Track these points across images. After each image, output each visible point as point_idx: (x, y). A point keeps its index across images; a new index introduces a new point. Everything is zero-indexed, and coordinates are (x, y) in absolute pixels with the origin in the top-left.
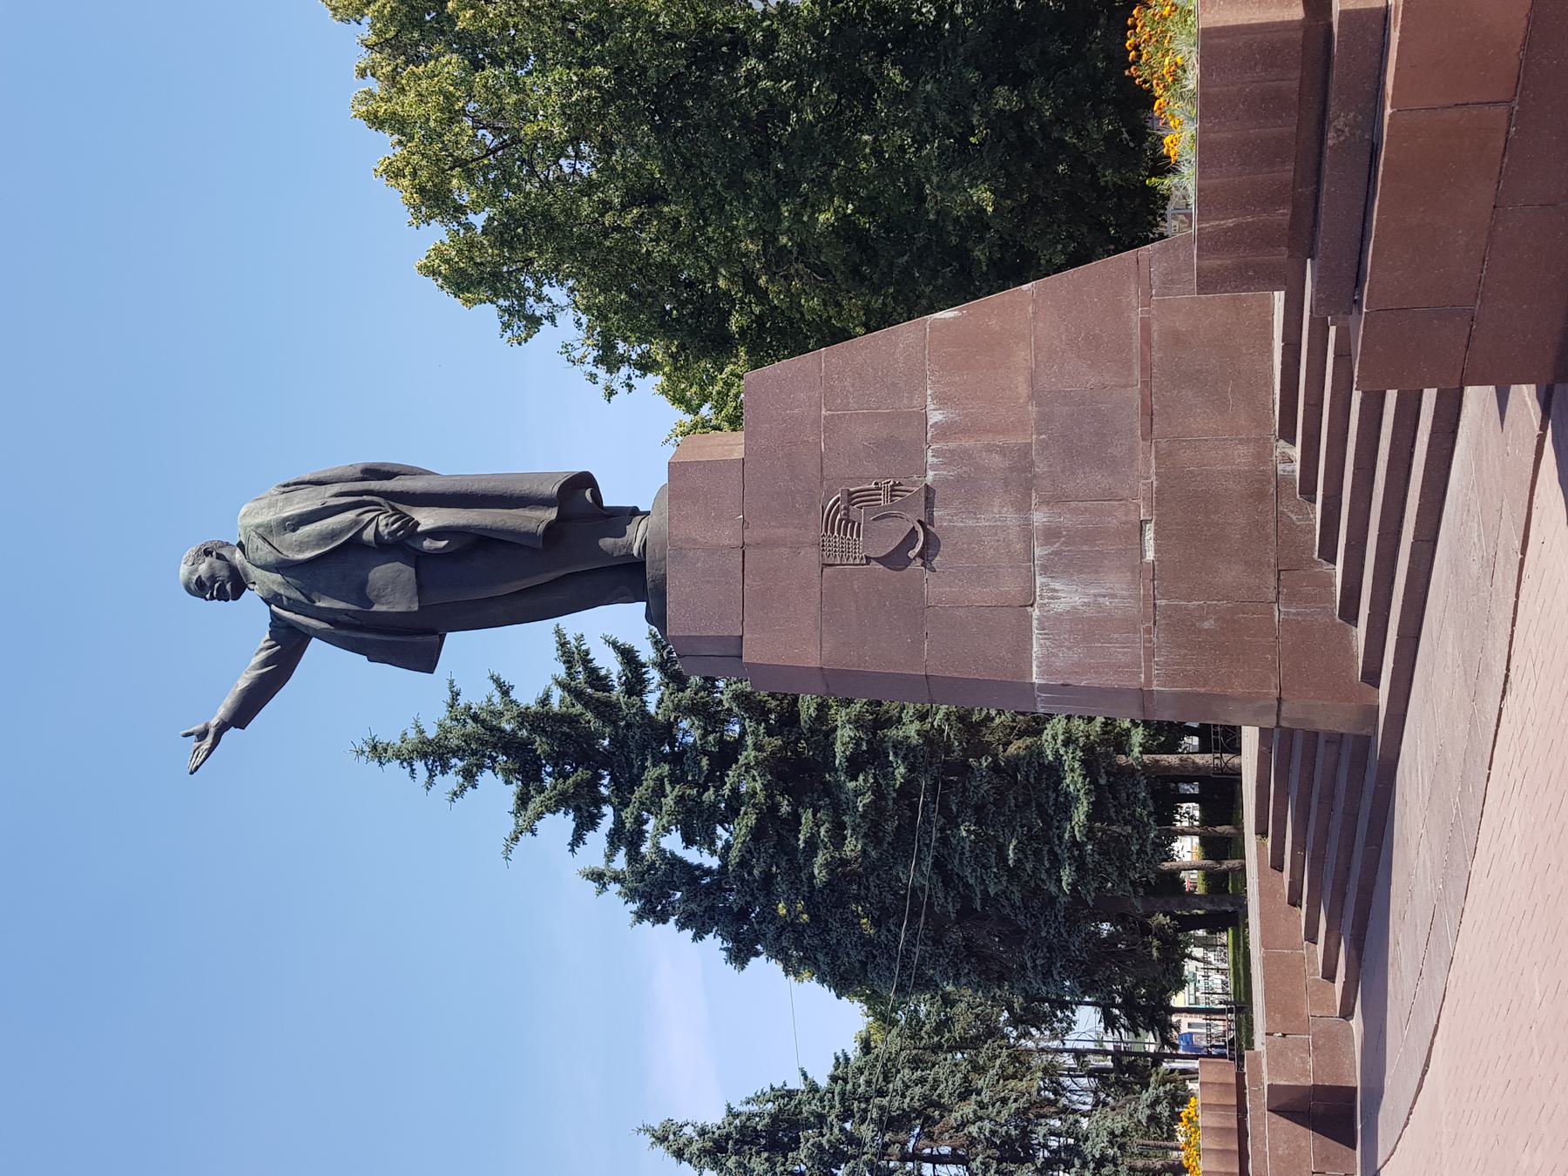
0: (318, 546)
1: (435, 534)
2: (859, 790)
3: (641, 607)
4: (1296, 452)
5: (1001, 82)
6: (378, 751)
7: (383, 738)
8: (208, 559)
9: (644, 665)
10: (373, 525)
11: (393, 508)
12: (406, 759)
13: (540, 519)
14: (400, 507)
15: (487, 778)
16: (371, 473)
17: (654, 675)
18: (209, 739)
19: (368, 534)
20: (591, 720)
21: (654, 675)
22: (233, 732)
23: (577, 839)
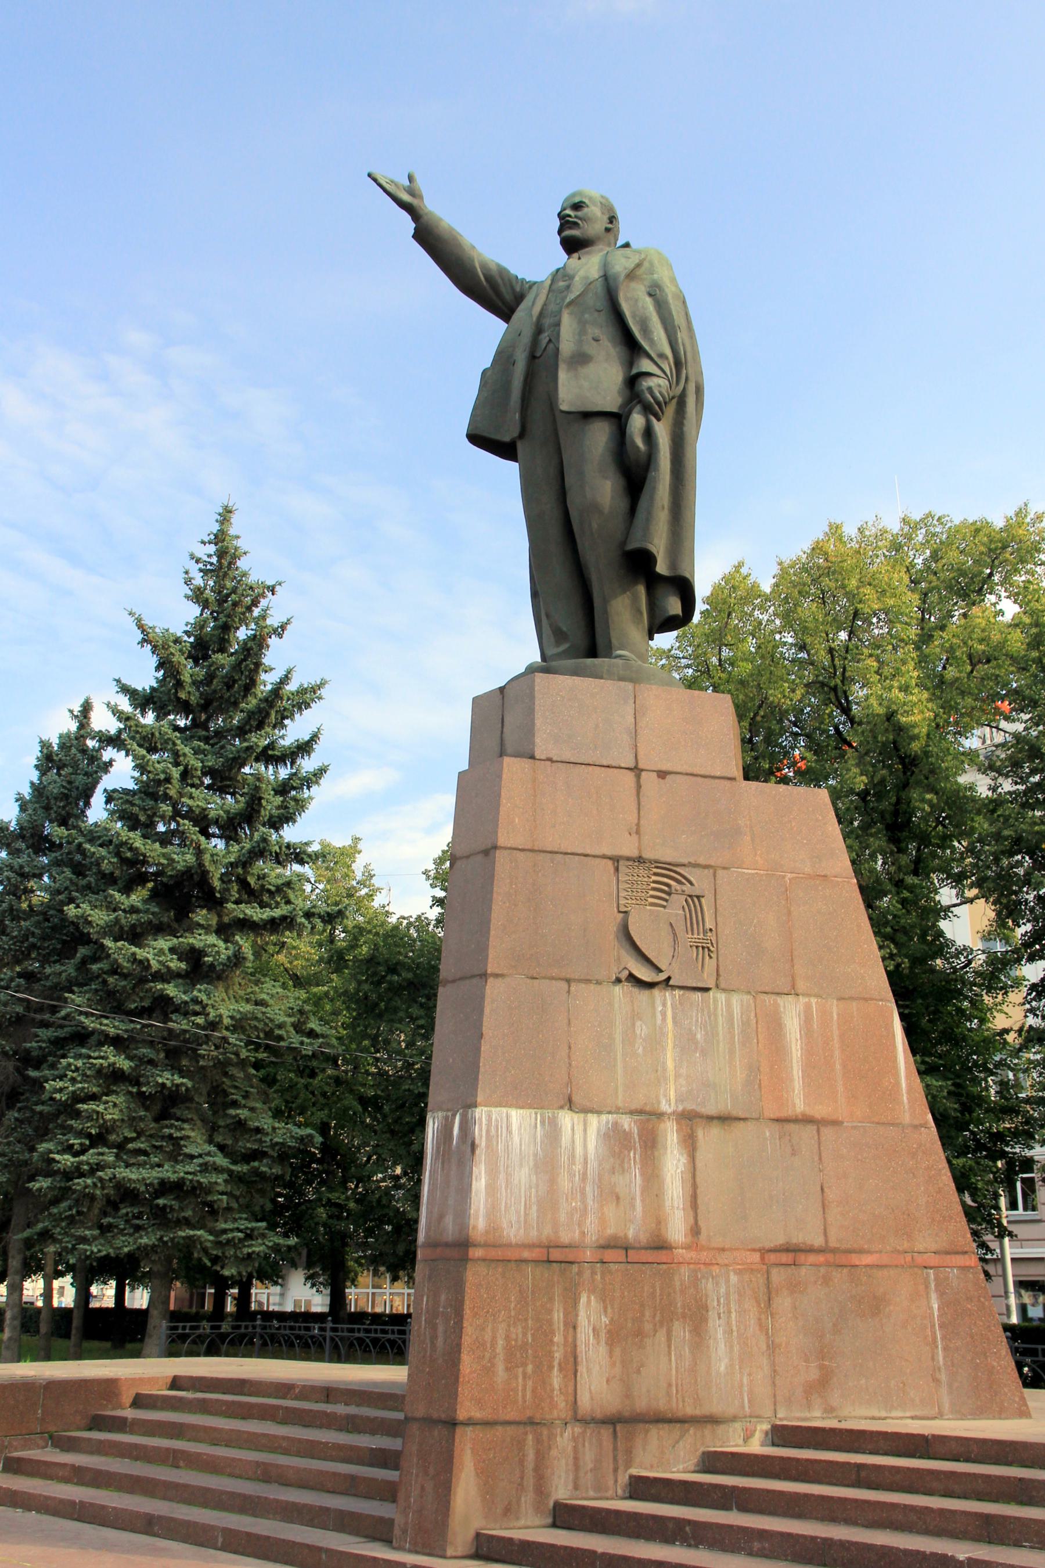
0: (634, 316)
1: (649, 434)
2: (158, 951)
3: (538, 658)
4: (756, 1447)
5: (177, 1278)
6: (226, 515)
7: (235, 519)
8: (605, 218)
9: (293, 763)
10: (658, 372)
11: (673, 398)
12: (219, 538)
13: (659, 546)
14: (675, 401)
15: (193, 611)
16: (699, 390)
17: (284, 772)
18: (405, 197)
19: (646, 366)
20: (251, 703)
21: (284, 772)
22: (409, 225)
23: (125, 689)
